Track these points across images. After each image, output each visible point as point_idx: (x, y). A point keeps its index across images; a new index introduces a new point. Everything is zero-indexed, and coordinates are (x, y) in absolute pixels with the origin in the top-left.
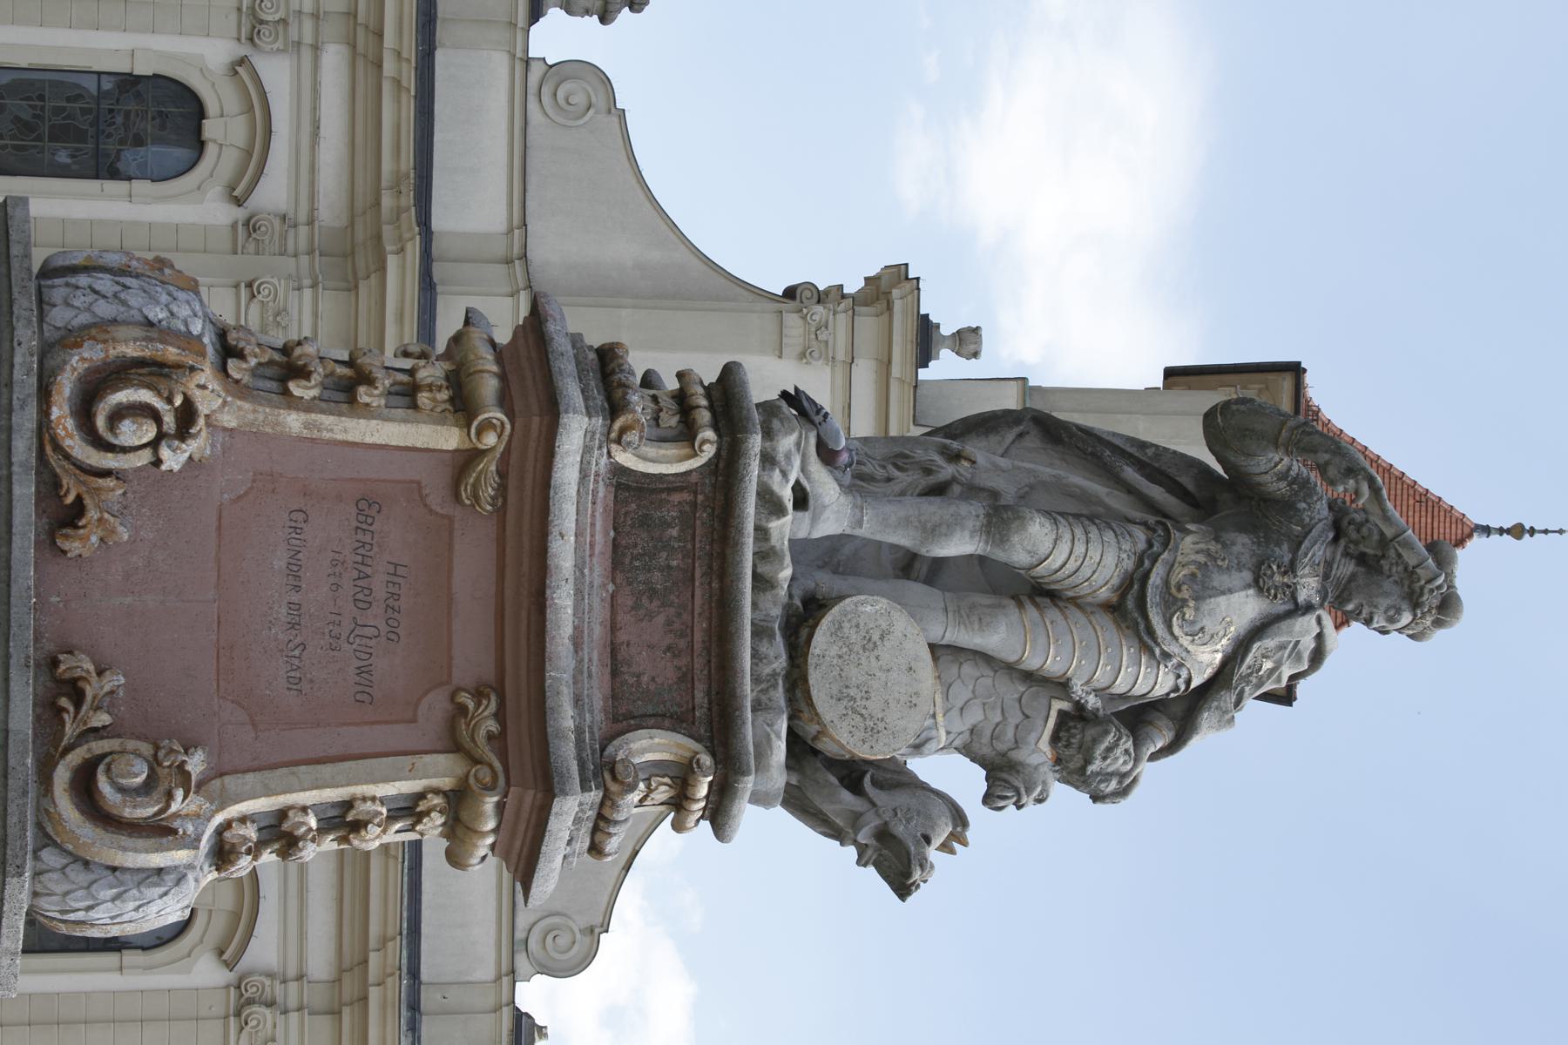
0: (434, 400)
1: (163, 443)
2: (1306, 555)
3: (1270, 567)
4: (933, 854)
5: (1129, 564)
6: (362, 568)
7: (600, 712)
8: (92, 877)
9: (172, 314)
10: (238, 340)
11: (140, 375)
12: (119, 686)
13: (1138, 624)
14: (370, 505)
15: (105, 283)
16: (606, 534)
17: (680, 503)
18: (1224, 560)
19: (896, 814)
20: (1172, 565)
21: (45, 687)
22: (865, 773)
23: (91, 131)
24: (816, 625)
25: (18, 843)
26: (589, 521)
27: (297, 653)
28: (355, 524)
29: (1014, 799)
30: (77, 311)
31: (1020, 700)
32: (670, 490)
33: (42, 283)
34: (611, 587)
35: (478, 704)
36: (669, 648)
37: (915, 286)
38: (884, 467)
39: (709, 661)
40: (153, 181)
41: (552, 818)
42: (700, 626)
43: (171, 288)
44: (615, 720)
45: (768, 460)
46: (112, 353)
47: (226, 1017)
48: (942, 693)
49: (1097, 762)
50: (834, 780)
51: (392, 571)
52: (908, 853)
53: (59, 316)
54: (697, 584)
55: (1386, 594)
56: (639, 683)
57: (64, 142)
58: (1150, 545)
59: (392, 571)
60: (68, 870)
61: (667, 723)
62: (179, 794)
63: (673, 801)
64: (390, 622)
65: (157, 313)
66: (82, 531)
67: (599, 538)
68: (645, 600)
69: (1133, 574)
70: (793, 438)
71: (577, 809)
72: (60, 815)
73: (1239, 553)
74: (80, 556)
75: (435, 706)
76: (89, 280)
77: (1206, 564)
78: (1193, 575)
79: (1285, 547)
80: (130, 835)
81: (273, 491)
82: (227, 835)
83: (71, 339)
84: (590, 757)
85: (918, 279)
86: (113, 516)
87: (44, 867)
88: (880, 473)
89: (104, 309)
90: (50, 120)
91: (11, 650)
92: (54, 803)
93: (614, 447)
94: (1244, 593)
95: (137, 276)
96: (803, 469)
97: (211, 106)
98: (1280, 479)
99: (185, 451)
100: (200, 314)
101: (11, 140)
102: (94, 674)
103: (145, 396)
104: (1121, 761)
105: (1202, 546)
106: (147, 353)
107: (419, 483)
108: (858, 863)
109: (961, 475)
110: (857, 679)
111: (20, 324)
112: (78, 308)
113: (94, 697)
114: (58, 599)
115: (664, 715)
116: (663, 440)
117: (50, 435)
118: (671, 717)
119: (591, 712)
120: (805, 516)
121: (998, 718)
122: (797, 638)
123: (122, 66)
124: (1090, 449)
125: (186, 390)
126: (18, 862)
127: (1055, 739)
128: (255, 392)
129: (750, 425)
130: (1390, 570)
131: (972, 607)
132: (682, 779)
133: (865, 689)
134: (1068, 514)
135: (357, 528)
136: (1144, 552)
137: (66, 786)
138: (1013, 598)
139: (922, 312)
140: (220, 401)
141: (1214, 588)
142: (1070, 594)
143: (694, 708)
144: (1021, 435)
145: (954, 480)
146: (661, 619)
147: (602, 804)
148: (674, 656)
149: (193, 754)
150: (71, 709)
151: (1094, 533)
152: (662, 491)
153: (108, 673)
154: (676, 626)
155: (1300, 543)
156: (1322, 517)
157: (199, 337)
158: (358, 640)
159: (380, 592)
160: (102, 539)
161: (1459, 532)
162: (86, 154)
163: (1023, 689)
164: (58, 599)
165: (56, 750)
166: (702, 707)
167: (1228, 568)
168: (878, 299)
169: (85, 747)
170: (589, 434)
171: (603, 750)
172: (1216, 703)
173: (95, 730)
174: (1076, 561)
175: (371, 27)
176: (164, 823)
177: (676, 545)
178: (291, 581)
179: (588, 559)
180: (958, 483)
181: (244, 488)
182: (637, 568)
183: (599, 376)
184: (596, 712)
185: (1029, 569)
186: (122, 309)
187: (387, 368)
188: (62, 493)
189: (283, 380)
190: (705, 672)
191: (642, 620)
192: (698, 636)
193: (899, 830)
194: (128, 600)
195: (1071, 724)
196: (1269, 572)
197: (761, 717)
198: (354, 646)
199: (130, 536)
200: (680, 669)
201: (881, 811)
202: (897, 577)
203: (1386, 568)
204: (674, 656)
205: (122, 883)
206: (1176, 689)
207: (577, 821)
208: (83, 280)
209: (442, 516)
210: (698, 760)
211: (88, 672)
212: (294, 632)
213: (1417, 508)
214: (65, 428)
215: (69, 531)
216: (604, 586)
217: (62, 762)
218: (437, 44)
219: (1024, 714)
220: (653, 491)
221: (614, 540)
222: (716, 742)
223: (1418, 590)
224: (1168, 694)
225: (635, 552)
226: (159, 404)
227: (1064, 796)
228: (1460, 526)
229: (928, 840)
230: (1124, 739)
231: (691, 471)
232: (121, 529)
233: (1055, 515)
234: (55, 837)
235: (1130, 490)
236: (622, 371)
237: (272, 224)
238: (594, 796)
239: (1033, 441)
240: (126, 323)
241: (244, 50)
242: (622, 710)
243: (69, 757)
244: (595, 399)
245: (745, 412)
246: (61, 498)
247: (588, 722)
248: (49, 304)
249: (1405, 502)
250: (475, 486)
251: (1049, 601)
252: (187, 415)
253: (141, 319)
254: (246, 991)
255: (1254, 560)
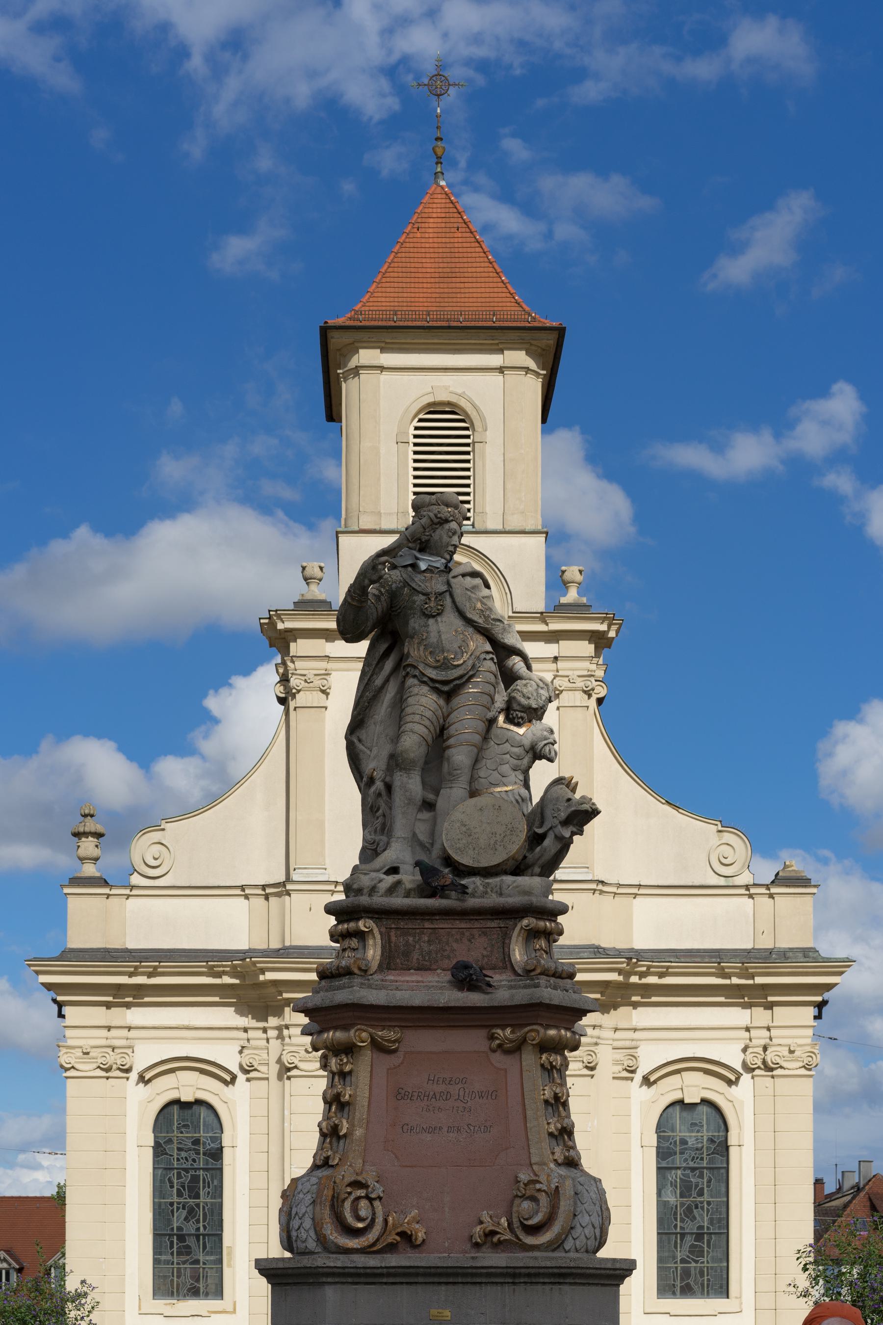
0: (347, 1063)
1: (370, 1195)
2: (420, 586)
3: (426, 608)
4: (578, 796)
5: (425, 689)
6: (430, 1097)
7: (501, 976)
8: (578, 1225)
9: (308, 1192)
10: (320, 1160)
11: (338, 1207)
12: (488, 1214)
13: (456, 684)
14: (400, 1093)
15: (295, 1223)
16: (412, 974)
17: (396, 937)
18: (423, 635)
19: (556, 817)
20: (426, 664)
21: (488, 1248)
22: (534, 832)
23: (192, 1172)
24: (458, 862)
25: (560, 1261)
26: (405, 983)
27: (472, 1128)
28: (408, 1101)
29: (551, 745)
30: (309, 1236)
31: (499, 744)
32: (390, 942)
33: (296, 1252)
34: (439, 971)
35: (497, 1038)
36: (469, 940)
37: (274, 613)
38: (378, 818)
39: (476, 920)
40: (222, 1133)
41: (552, 1003)
42: (459, 924)
43: (296, 1192)
44: (506, 968)
45: (373, 890)
46: (328, 1220)
47: (773, 1077)
48: (495, 788)
49: (531, 702)
50: (538, 849)
51: (432, 1082)
52: (575, 811)
53: (312, 1245)
54: (437, 927)
55: (441, 538)
56: (487, 956)
57: (199, 1190)
58: (415, 676)
59: (432, 1082)
60: (575, 1237)
61: (507, 941)
62: (538, 1186)
63: (547, 937)
64: (457, 1082)
65: (308, 1199)
66: (413, 1233)
67: (414, 978)
68: (445, 954)
69: (431, 687)
70: (362, 876)
71: (549, 989)
72: (548, 1241)
73: (419, 626)
74: (425, 1233)
75: (498, 1059)
76: (293, 1230)
77: (425, 645)
78: (431, 653)
79: (415, 598)
80: (559, 1208)
81: (393, 1141)
82: (560, 1161)
83: (321, 1240)
84: (523, 982)
85: (269, 611)
86: (406, 1217)
87: (574, 1247)
88: (380, 820)
89: (308, 1223)
90: (186, 1198)
91: (468, 1266)
92: (543, 1244)
93: (369, 973)
94: (440, 623)
95: (291, 1208)
96: (378, 871)
97: (677, 1096)
98: (380, 600)
99: (374, 1185)
100: (308, 1178)
101: (199, 1223)
102: (482, 1226)
103: (347, 1205)
104: (530, 689)
105: (416, 646)
106: (328, 1204)
107: (388, 1069)
108: (581, 834)
109: (381, 777)
110: (485, 840)
111: (315, 1263)
112: (307, 1236)
113: (493, 1225)
114: (446, 1243)
115: (504, 943)
116: (364, 947)
117: (367, 1248)
118: (504, 939)
119: (501, 981)
120: (403, 868)
121: (508, 756)
122: (465, 871)
123: (149, 1153)
124: (366, 704)
125: (344, 1186)
126: (569, 1261)
127: (518, 725)
128: (345, 1151)
129: (356, 902)
130: (427, 536)
131: (450, 774)
132: (533, 934)
133: (491, 835)
134: (399, 724)
135: (411, 1099)
136: (419, 680)
137: (535, 1238)
138: (444, 751)
139: (292, 607)
140: (349, 1168)
141: (437, 642)
142: (441, 721)
143: (500, 927)
144: (360, 741)
145: (383, 781)
146: (455, 945)
147: (547, 975)
148: (473, 938)
149: (520, 1179)
150: (498, 1236)
151: (409, 710)
152: (390, 946)
153: (481, 1219)
154: (458, 937)
155: (414, 589)
156: (399, 575)
157: (320, 1179)
158: (466, 1098)
159: (442, 1088)
160: (418, 1223)
161: (439, 196)
162: (206, 1175)
163: (493, 743)
164: (446, 1243)
165: (518, 1243)
166: (499, 923)
167: (427, 633)
168: (284, 638)
169: (516, 1230)
170: (362, 985)
171: (521, 976)
172: (500, 635)
173: (509, 1224)
174: (424, 720)
175: (115, 992)
176: (553, 1192)
177: (417, 938)
178: (437, 1131)
179: (425, 984)
180: (385, 778)
181: (392, 1155)
182: (429, 958)
183: (333, 980)
184: (501, 978)
185: (429, 745)
186: (307, 1215)
187: (332, 1086)
188: (395, 1242)
189: (339, 1138)
190: (482, 921)
191: (455, 955)
192: (463, 925)
193: (563, 815)
194: (447, 1209)
195: (511, 716)
196: (429, 609)
197: (505, 891)
198: (469, 1100)
199: (416, 1209)
200: (480, 935)
201: (554, 825)
202: (434, 810)
203: (427, 538)
204: (473, 938)
205: (581, 1212)
206: (492, 659)
207: (555, 988)
208: (294, 1234)
209: (405, 1057)
210: (525, 926)
211: (481, 1229)
212: (462, 1129)
213: (423, 230)
214: (364, 1241)
215: (414, 1238)
216: (438, 975)
217: (523, 1240)
218: (123, 947)
219: (505, 743)
220: (390, 951)
221: (415, 970)
222: (516, 916)
223: (438, 520)
224: (495, 663)
225: (421, 959)
226: (352, 1197)
227: (551, 718)
228: (436, 196)
229: (569, 800)
230: (518, 687)
231: (380, 931)
232: (412, 1214)
233: (400, 733)
234: (559, 1244)
235: (387, 680)
236: (331, 968)
237: (248, 1055)
238: (543, 980)
239: (363, 734)
240: (314, 1214)
241: (134, 1076)
242: (501, 964)
243: (521, 1237)
244: (344, 983)
245: (349, 905)
246: (398, 1242)
247: (507, 983)
248: (306, 1249)
249: (419, 240)
250: (389, 1041)
251: (445, 731)
252: (357, 1184)
253: (311, 1207)
254: (756, 1064)
255: (423, 618)
